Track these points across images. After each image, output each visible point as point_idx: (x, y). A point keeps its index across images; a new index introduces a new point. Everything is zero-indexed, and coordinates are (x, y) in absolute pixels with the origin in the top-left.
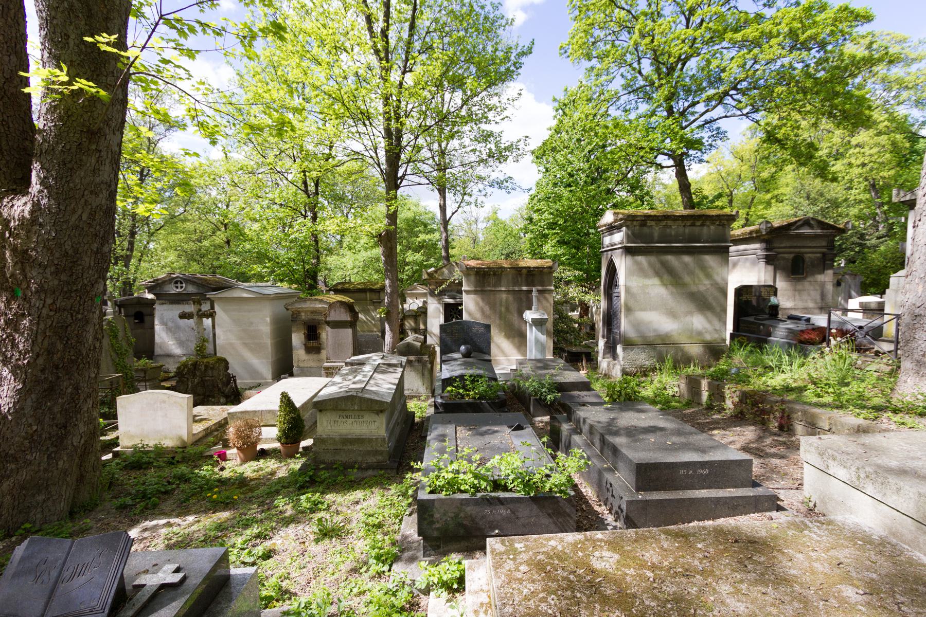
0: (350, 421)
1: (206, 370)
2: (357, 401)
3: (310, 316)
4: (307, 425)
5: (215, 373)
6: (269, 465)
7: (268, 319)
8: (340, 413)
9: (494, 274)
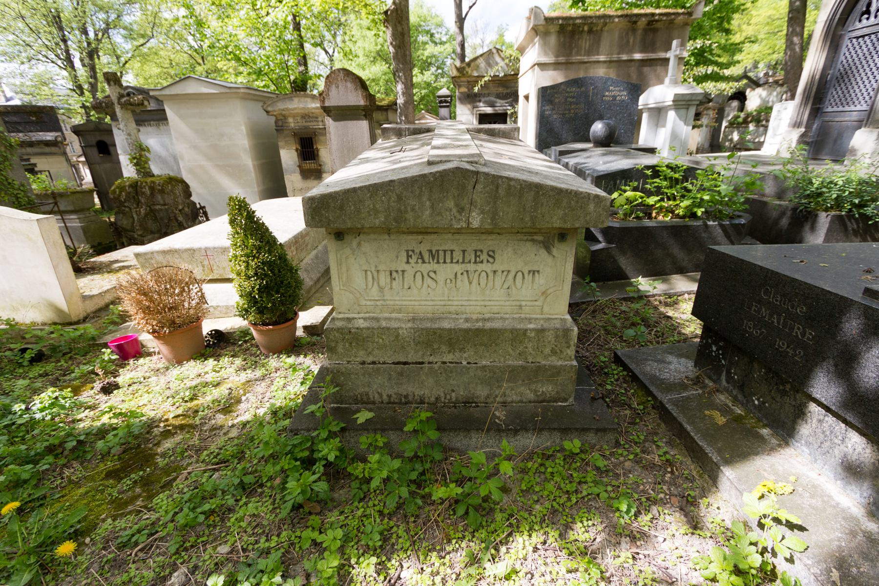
0: (446, 271)
1: (152, 194)
2: (479, 195)
3: (302, 123)
4: (307, 278)
5: (169, 200)
6: (227, 372)
7: (243, 128)
8: (412, 242)
9: (590, 31)
